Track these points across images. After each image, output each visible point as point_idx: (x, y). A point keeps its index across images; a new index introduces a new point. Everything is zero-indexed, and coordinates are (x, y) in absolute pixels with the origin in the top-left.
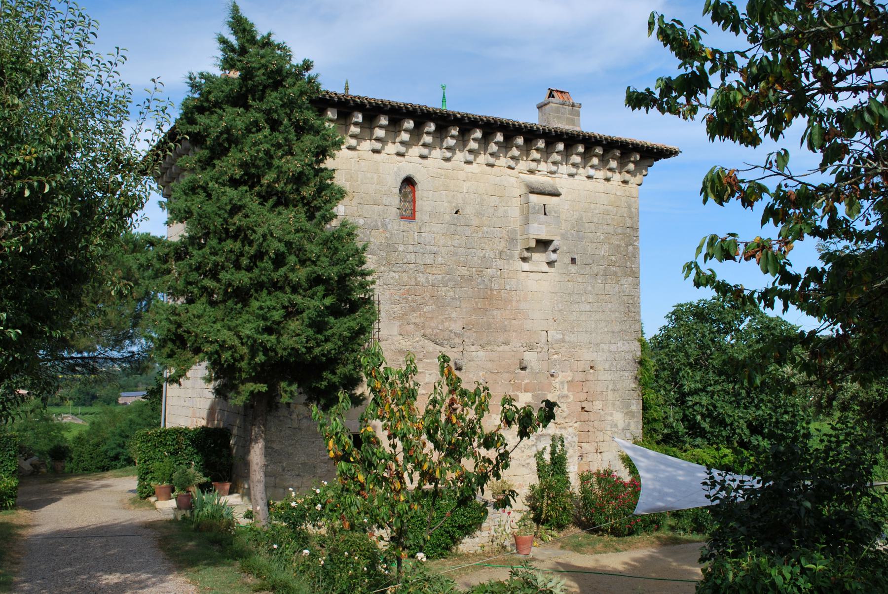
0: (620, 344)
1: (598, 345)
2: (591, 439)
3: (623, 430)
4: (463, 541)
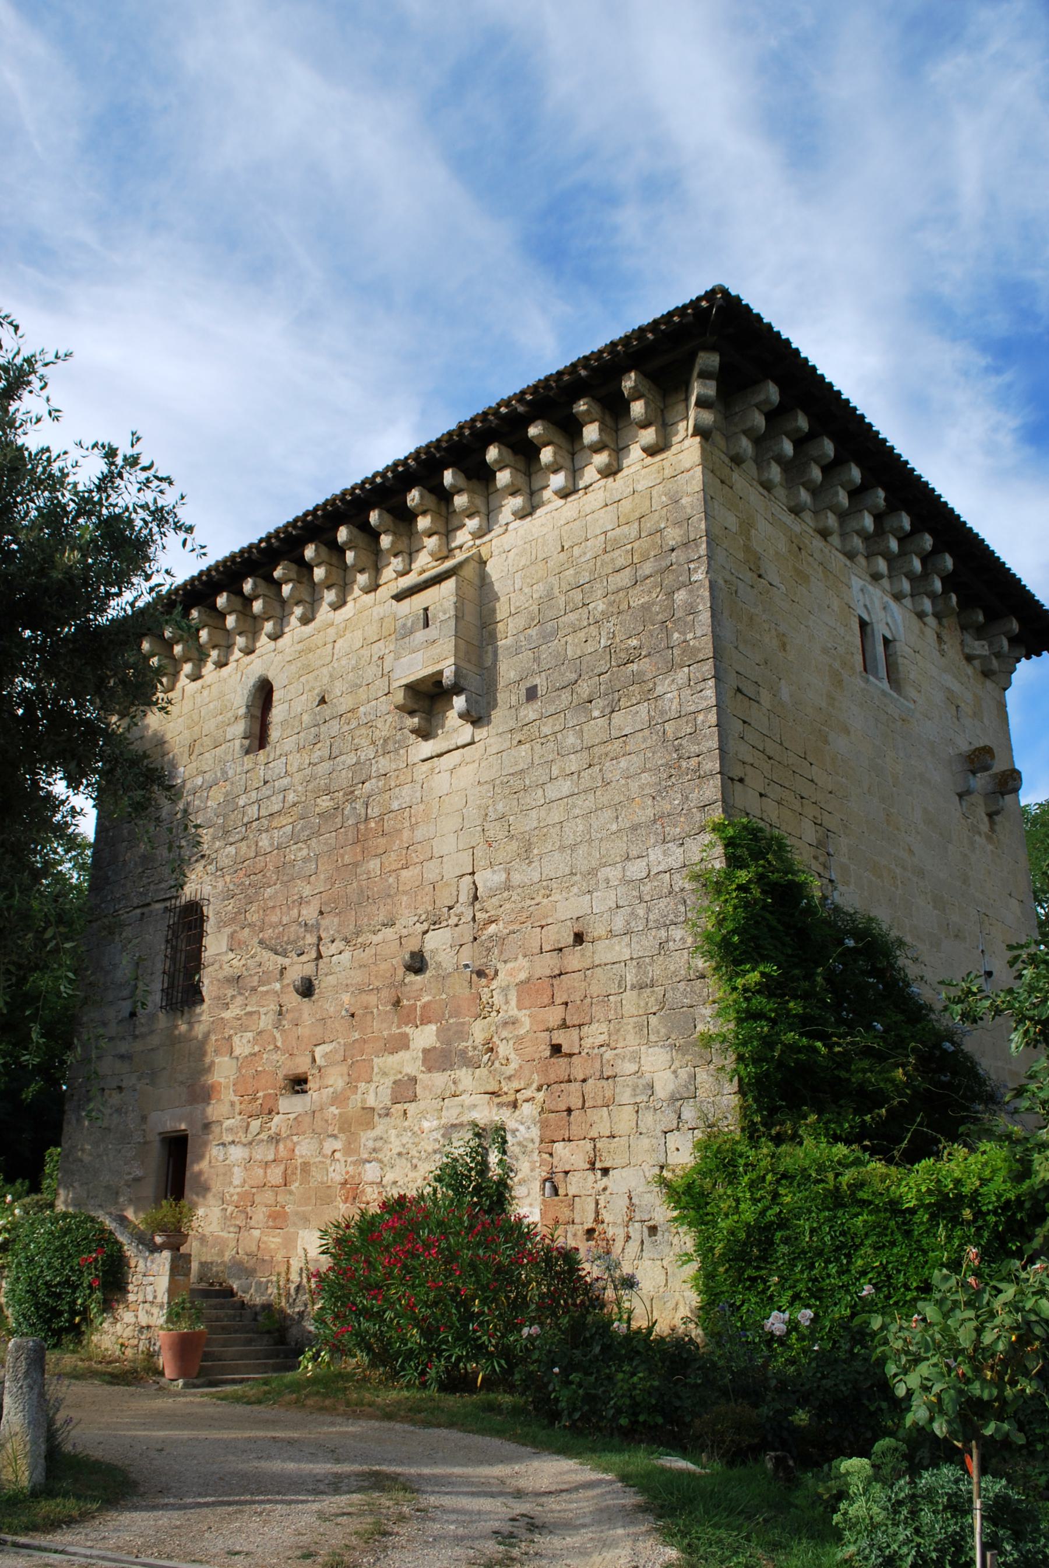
0: (655, 855)
1: (593, 872)
3: (674, 1099)
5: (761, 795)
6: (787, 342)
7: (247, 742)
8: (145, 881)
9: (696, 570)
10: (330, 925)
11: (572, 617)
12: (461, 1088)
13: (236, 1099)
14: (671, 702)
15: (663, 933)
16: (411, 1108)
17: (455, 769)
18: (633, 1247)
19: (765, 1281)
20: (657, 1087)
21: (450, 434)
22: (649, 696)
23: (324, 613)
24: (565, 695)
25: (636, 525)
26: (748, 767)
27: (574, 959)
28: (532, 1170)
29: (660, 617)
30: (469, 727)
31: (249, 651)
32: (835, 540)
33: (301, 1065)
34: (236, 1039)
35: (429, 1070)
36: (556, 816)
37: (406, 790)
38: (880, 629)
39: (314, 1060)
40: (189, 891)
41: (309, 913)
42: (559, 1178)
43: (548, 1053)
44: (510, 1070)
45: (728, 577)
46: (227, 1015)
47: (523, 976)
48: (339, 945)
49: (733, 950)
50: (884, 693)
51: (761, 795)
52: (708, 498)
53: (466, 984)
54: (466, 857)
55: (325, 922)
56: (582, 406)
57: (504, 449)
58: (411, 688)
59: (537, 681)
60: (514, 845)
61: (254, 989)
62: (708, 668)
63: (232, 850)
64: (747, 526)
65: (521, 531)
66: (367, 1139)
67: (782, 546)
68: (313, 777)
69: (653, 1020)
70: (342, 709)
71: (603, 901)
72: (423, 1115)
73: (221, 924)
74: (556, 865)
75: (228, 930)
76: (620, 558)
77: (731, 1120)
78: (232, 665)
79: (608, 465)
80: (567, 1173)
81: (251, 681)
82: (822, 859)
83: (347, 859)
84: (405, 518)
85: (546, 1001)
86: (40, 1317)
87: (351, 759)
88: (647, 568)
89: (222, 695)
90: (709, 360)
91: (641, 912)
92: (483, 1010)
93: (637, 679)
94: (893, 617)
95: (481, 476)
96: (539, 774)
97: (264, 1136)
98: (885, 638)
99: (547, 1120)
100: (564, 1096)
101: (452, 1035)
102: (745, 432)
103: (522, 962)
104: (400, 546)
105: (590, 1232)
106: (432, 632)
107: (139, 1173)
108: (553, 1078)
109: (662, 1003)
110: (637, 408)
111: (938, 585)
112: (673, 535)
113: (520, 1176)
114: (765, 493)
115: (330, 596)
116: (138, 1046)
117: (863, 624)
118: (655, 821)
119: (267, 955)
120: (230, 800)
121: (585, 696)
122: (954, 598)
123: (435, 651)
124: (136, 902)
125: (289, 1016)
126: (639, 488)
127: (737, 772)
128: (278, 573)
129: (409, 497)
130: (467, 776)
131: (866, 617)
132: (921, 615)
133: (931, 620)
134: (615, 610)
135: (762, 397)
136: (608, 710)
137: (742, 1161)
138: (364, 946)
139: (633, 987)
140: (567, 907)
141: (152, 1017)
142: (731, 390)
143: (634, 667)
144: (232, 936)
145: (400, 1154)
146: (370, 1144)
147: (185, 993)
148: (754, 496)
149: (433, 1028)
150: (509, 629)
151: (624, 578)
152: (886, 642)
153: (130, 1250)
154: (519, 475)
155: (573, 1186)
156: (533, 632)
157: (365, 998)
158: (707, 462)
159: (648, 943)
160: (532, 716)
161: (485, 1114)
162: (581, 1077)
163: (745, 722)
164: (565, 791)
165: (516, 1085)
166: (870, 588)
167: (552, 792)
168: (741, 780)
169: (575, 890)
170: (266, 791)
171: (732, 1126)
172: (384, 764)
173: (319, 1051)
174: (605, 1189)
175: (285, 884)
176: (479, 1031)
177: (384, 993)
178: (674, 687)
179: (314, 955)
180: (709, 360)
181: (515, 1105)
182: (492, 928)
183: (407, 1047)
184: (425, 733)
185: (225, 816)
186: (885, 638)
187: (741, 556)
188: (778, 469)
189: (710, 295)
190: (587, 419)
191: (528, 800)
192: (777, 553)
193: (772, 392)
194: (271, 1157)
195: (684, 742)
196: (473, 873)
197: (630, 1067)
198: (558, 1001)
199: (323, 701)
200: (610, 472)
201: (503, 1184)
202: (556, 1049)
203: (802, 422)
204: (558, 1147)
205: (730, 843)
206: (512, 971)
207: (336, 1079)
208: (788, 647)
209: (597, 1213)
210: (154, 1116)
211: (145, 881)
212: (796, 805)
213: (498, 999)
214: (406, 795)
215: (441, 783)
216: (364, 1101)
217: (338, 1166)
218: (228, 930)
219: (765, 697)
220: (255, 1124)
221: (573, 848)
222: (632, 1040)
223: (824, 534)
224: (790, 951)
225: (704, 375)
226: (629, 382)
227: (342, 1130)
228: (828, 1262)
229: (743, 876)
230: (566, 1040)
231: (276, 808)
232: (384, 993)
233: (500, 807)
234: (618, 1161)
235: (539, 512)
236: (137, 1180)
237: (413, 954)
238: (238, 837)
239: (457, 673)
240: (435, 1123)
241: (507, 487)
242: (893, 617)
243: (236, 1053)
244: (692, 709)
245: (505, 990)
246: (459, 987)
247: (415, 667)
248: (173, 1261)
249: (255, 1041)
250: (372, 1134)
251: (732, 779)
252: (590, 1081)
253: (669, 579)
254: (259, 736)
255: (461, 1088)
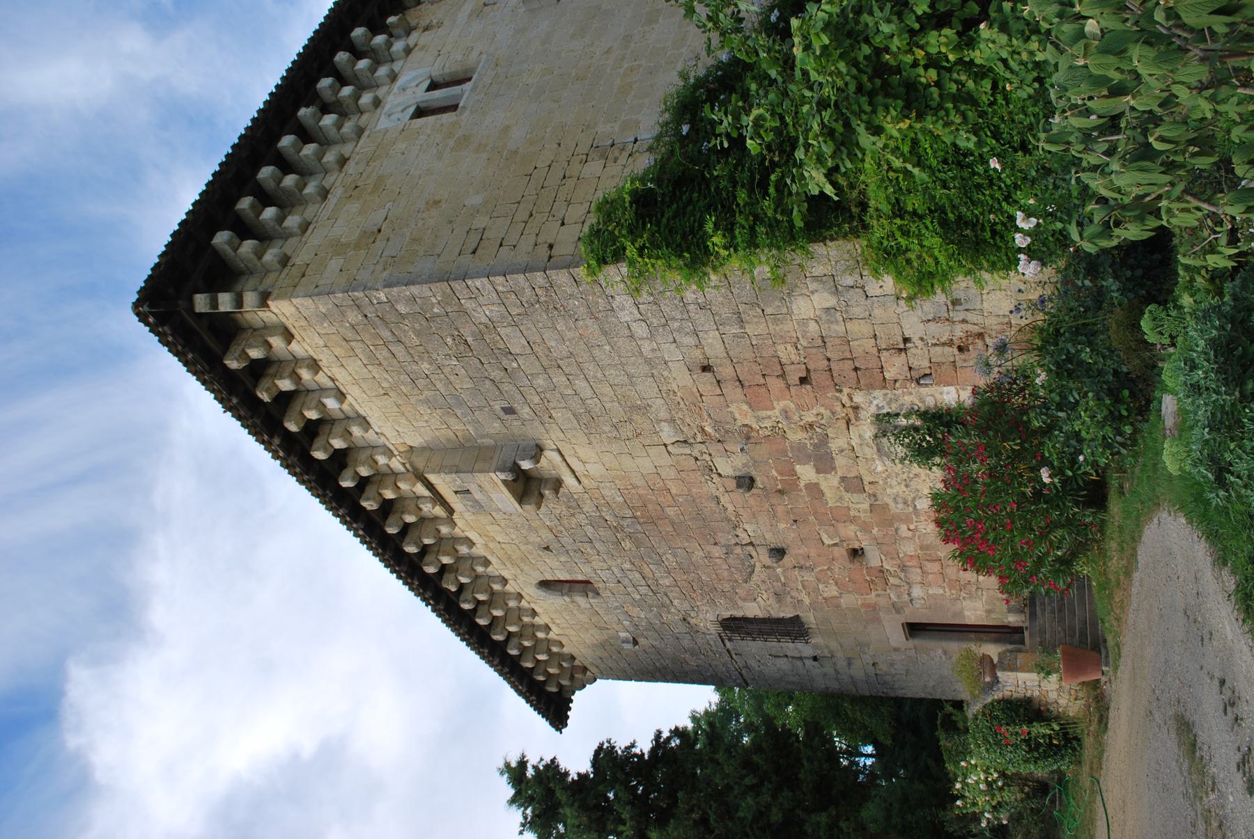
0: (625, 317)
1: (648, 361)
2: (873, 363)
3: (836, 291)
4: (1225, 573)
5: (563, 224)
6: (174, 235)
7: (590, 594)
8: (710, 653)
9: (378, 299)
10: (722, 538)
11: (439, 385)
12: (846, 446)
13: (874, 593)
14: (494, 311)
15: (691, 307)
16: (867, 479)
17: (584, 461)
18: (970, 317)
19: (995, 224)
20: (828, 305)
21: (309, 489)
22: (492, 326)
23: (479, 550)
24: (505, 387)
25: (353, 344)
26: (540, 240)
27: (726, 371)
28: (911, 394)
29: (424, 323)
30: (547, 453)
31: (520, 597)
32: (347, 149)
33: (840, 553)
34: (825, 595)
35: (834, 468)
36: (607, 390)
37: (606, 492)
38: (420, 95)
39: (836, 545)
40: (714, 629)
41: (717, 552)
42: (915, 374)
43: (808, 387)
44: (827, 413)
45: (380, 267)
46: (807, 601)
47: (745, 407)
48: (739, 532)
49: (695, 256)
50: (474, 89)
51: (563, 224)
52: (317, 292)
53: (758, 447)
54: (652, 451)
55: (723, 541)
56: (265, 397)
57: (314, 447)
58: (521, 498)
59: (497, 407)
60: (635, 417)
61: (784, 585)
62: (457, 285)
63: (676, 602)
64: (339, 248)
65: (380, 423)
66: (896, 508)
67: (354, 207)
68: (608, 553)
69: (768, 311)
70: (550, 536)
71: (671, 353)
72: (872, 472)
73: (735, 605)
74: (647, 388)
75: (740, 603)
76: (382, 354)
77: (849, 246)
78: (533, 606)
79: (308, 367)
80: (910, 368)
81: (541, 593)
82: (617, 153)
83: (670, 529)
84: (387, 508)
85: (763, 390)
86: (1055, 754)
87: (589, 530)
88: (386, 334)
89: (556, 611)
90: (201, 303)
91: (676, 325)
92: (777, 433)
93: (480, 336)
94: (410, 81)
95: (341, 459)
96: (575, 403)
97: (902, 575)
98: (428, 90)
99: (866, 385)
100: (844, 374)
101: (802, 454)
102: (260, 258)
103: (733, 408)
104: (413, 507)
105: (960, 349)
106: (473, 488)
107: (940, 651)
108: (829, 382)
109: (753, 305)
110: (255, 354)
111: (380, 39)
112: (353, 316)
113: (917, 402)
114: (311, 227)
115: (463, 550)
116: (839, 655)
117: (420, 113)
118: (596, 318)
119: (755, 577)
120: (635, 603)
121: (502, 374)
122: (391, 19)
123: (487, 486)
124: (727, 658)
125: (802, 562)
126: (321, 343)
127: (543, 251)
128: (453, 589)
129: (369, 508)
130: (584, 452)
131: (412, 110)
132: (408, 51)
133: (412, 40)
134: (426, 355)
135: (227, 247)
136: (510, 357)
137: (885, 243)
138: (738, 515)
139: (742, 327)
140: (681, 378)
141: (816, 647)
142: (224, 275)
143: (470, 340)
144: (744, 600)
145: (907, 486)
146: (900, 506)
147: (793, 628)
148: (314, 239)
149: (798, 468)
150: (459, 427)
151: (399, 350)
152: (434, 86)
153: (997, 695)
154: (334, 430)
155: (921, 363)
156: (459, 412)
157: (779, 514)
158: (287, 295)
159: (701, 318)
160: (527, 410)
161: (867, 429)
162: (826, 362)
163: (501, 245)
164: (584, 384)
165: (838, 408)
166: (387, 107)
167: (588, 393)
168: (551, 247)
169: (666, 373)
170: (626, 582)
171: (858, 246)
172: (588, 507)
173: (827, 541)
174: (922, 339)
175: (696, 568)
176: (796, 436)
177: (774, 501)
178: (479, 309)
179: (750, 548)
180: (201, 303)
181: (856, 408)
182: (708, 429)
183: (817, 484)
184: (557, 484)
185: (650, 606)
186: (428, 90)
187: (363, 252)
188: (289, 218)
189: (143, 318)
190: (274, 389)
191: (597, 410)
192: (360, 213)
193: (221, 238)
194: (919, 570)
195: (524, 300)
196: (665, 445)
197: (813, 326)
198: (762, 381)
199: (547, 548)
200: (315, 366)
201: (924, 415)
202: (803, 381)
203: (245, 203)
204: (887, 375)
205: (603, 261)
206: (742, 414)
207: (850, 531)
208: (437, 198)
209: (944, 344)
210: (893, 643)
211: (710, 653)
212: (570, 183)
213: (768, 423)
214: (609, 492)
215: (595, 469)
216: (865, 511)
217: (921, 526)
218: (740, 603)
219: (480, 222)
220: (892, 580)
221: (630, 376)
222: (787, 326)
223: (343, 161)
224: (696, 195)
225: (214, 303)
226: (233, 364)
227: (891, 525)
228: (974, 173)
229: (631, 251)
230: (794, 376)
231: (638, 575)
232: (774, 501)
233: (607, 429)
234: (897, 331)
235: (362, 412)
236: (945, 653)
237: (739, 486)
238: (665, 598)
239: (502, 470)
240: (877, 462)
241: (345, 440)
242: (407, 84)
243: (836, 593)
244: (494, 295)
245: (759, 419)
246: (763, 451)
247: (504, 499)
248: (1004, 670)
249: (826, 583)
250: (892, 505)
251: (550, 257)
252: (828, 355)
253: (391, 318)
254: (585, 587)
255: (846, 446)
